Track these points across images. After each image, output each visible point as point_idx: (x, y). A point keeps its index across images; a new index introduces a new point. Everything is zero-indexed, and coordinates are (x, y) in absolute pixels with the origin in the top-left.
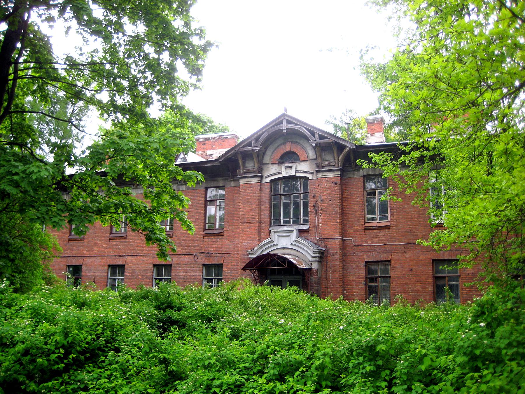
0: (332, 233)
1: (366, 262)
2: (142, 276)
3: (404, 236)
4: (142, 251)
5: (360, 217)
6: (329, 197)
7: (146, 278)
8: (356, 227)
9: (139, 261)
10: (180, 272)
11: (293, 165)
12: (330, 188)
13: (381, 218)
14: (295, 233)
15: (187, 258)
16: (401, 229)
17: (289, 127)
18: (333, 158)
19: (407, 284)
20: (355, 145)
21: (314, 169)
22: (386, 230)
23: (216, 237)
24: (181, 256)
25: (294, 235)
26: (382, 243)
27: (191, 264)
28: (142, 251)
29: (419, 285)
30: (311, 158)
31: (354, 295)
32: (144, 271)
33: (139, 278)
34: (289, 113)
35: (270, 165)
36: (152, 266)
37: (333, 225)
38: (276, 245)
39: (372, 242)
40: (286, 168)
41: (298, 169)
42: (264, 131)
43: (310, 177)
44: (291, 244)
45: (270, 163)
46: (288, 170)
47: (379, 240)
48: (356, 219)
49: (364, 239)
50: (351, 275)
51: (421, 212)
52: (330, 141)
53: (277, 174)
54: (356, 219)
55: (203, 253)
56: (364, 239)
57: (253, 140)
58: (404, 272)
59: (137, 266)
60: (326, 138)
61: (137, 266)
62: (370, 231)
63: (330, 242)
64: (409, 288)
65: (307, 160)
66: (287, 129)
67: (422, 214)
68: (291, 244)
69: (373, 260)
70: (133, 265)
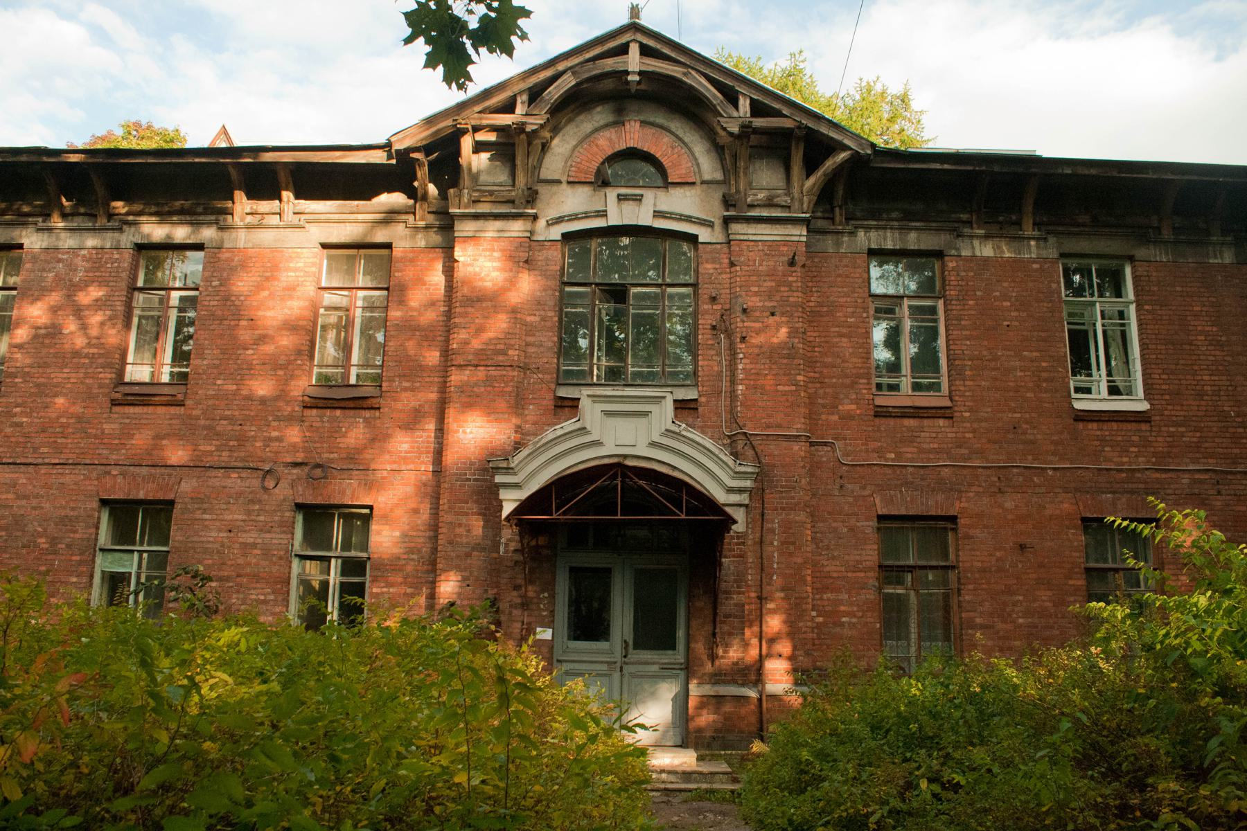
0: (779, 418)
1: (881, 518)
2: (54, 541)
3: (995, 442)
4: (58, 449)
5: (859, 376)
6: (768, 304)
7: (69, 546)
8: (847, 407)
9: (46, 486)
10: (206, 528)
11: (649, 195)
12: (771, 274)
13: (916, 387)
14: (669, 405)
15: (234, 481)
16: (986, 420)
17: (650, 69)
18: (782, 184)
19: (1009, 591)
20: (873, 146)
21: (715, 212)
22: (941, 422)
23: (352, 412)
24: (213, 473)
25: (665, 413)
26: (929, 460)
27: (252, 502)
28: (58, 449)
29: (1044, 595)
30: (707, 177)
31: (842, 625)
32: (63, 521)
33: (36, 545)
34: (645, 21)
35: (564, 185)
36: (95, 504)
37: (785, 393)
38: (597, 443)
39: (899, 455)
40: (621, 198)
41: (663, 207)
42: (561, 67)
43: (704, 235)
44: (654, 444)
45: (564, 179)
46: (628, 207)
47: (921, 451)
48: (848, 381)
49: (872, 445)
50: (834, 558)
51: (1044, 375)
52: (787, 124)
53: (587, 216)
54: (848, 381)
55: (296, 465)
56: (872, 445)
57: (521, 93)
58: (998, 554)
59: (34, 502)
60: (778, 114)
61: (34, 502)
62: (891, 422)
63: (773, 447)
64: (1015, 604)
65: (693, 184)
66: (641, 73)
67: (1046, 380)
68: (654, 444)
69: (903, 512)
70: (18, 498)
